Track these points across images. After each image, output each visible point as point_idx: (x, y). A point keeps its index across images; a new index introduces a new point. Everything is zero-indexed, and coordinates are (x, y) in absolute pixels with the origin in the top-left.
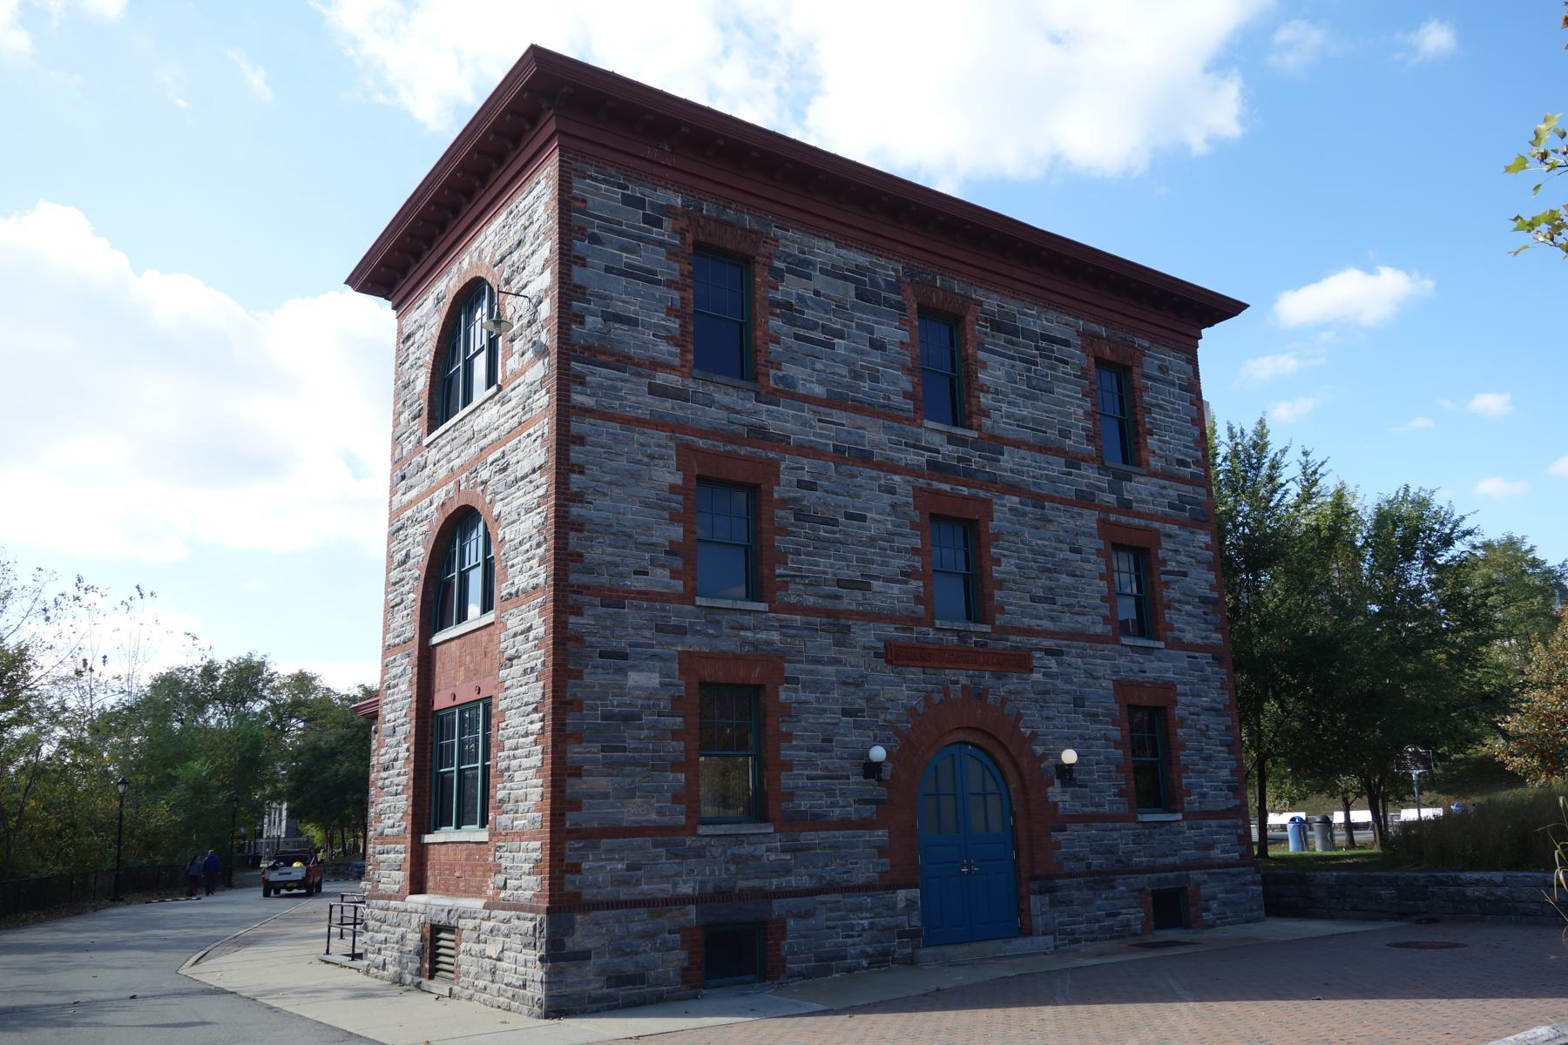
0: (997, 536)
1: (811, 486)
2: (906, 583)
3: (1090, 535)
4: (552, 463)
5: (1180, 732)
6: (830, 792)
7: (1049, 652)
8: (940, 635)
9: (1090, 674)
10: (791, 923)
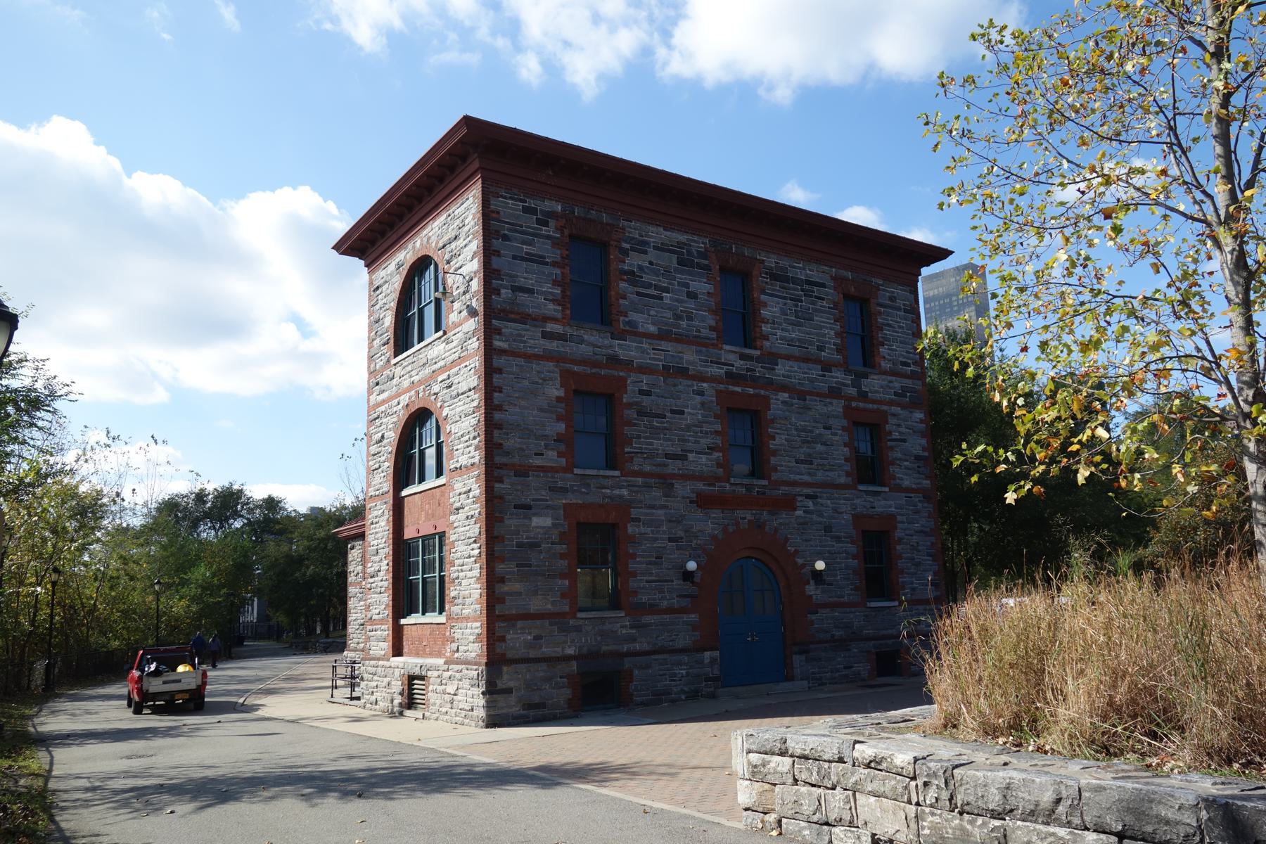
0: (772, 421)
1: (648, 393)
3: (836, 417)
4: (482, 386)
5: (898, 547)
7: (808, 497)
9: (836, 511)
10: (636, 672)
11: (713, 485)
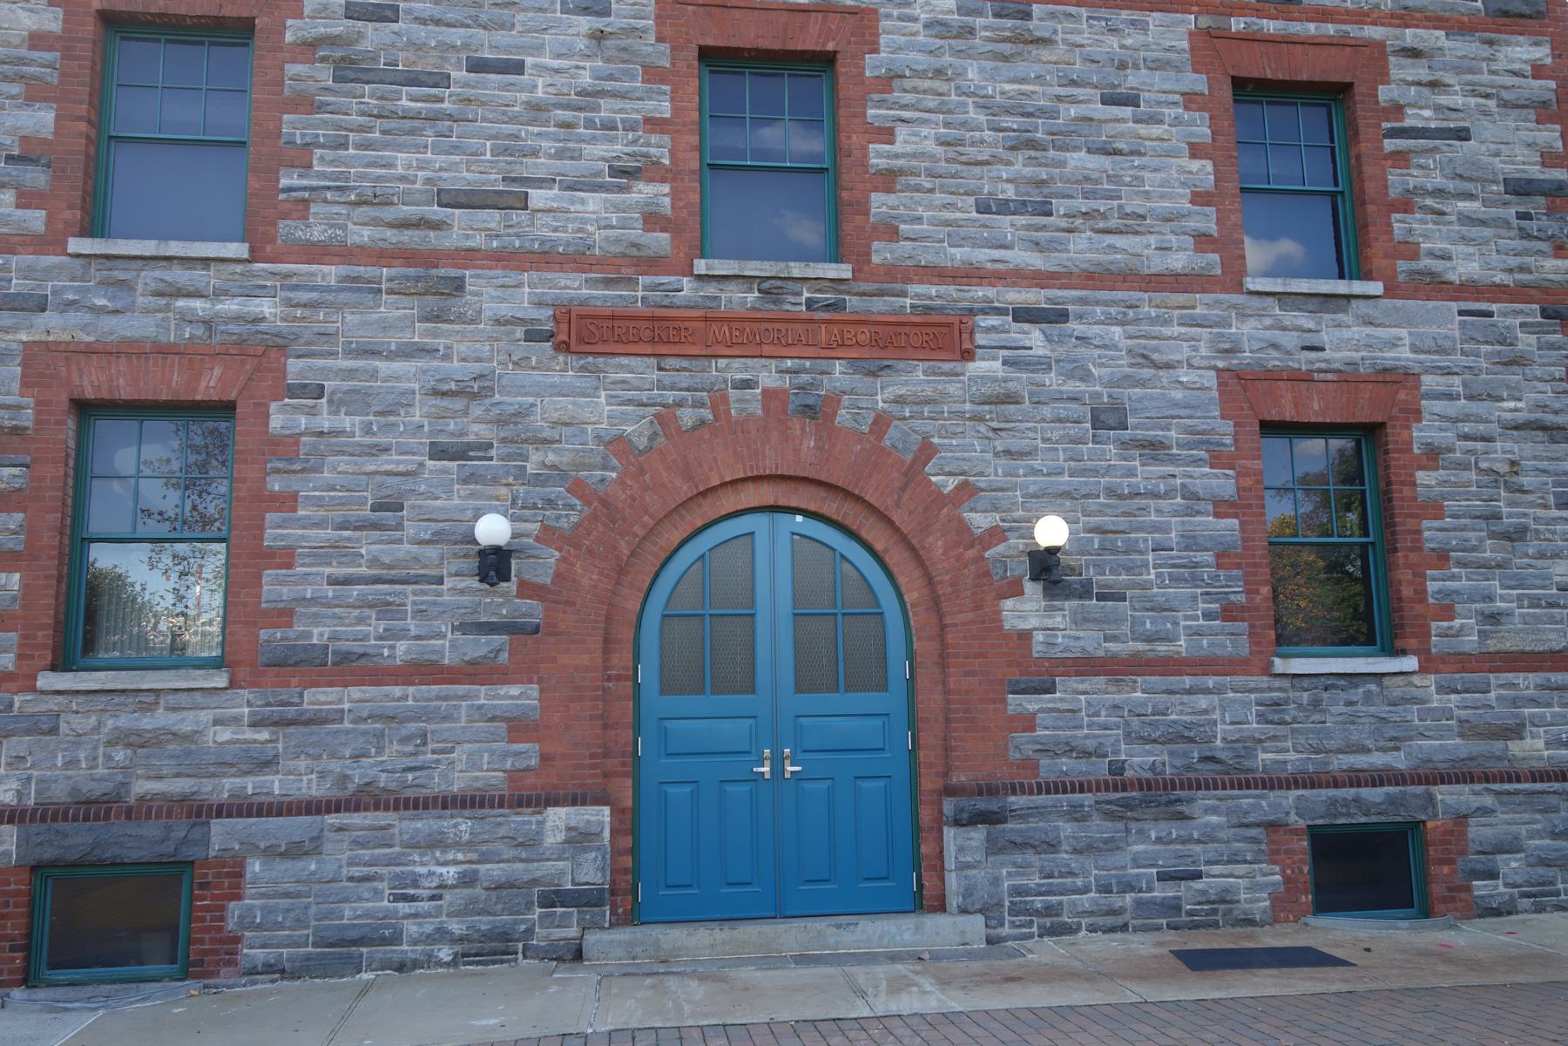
0: (888, 82)
2: (621, 189)
5: (1422, 477)
6: (386, 609)
7: (1024, 315)
8: (711, 290)
10: (255, 866)
11: (631, 282)
